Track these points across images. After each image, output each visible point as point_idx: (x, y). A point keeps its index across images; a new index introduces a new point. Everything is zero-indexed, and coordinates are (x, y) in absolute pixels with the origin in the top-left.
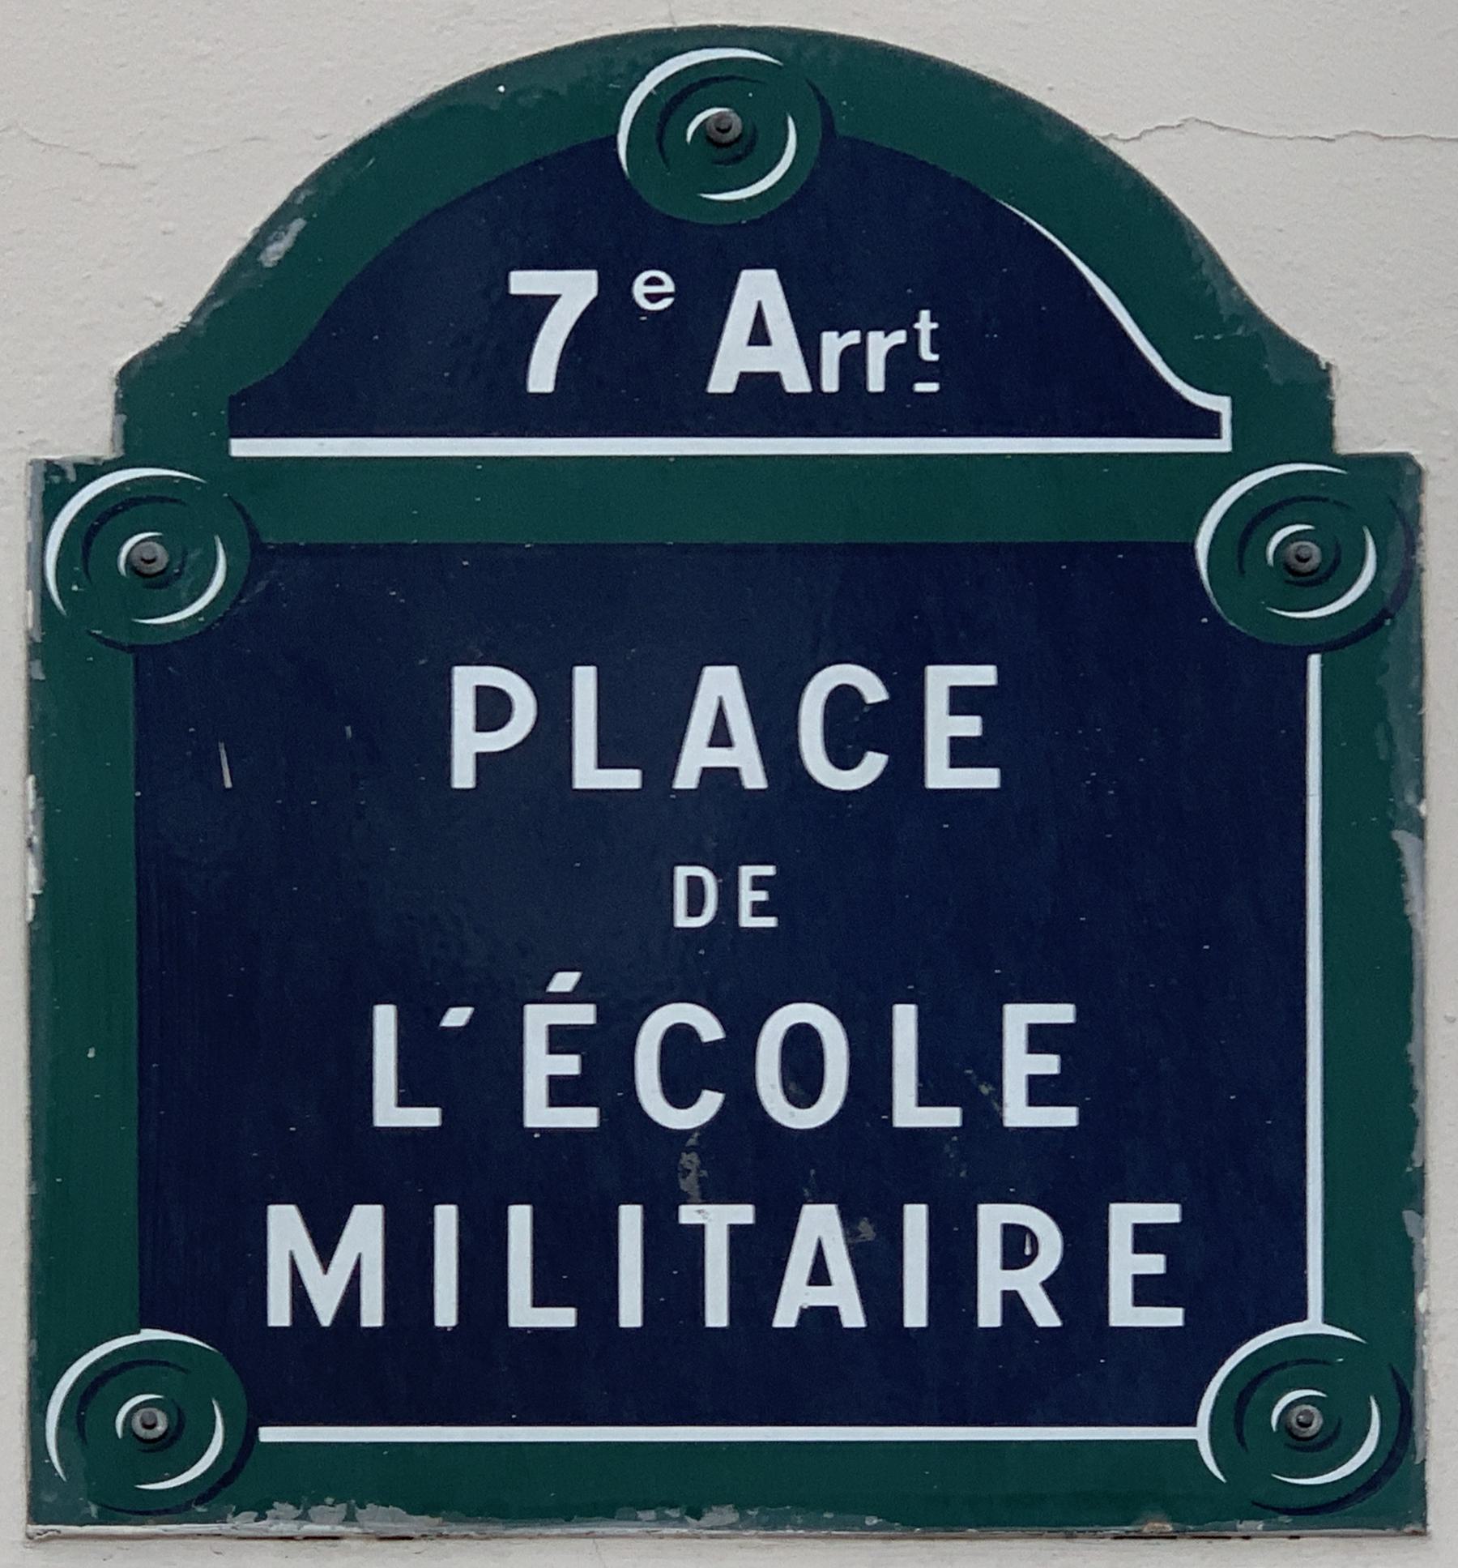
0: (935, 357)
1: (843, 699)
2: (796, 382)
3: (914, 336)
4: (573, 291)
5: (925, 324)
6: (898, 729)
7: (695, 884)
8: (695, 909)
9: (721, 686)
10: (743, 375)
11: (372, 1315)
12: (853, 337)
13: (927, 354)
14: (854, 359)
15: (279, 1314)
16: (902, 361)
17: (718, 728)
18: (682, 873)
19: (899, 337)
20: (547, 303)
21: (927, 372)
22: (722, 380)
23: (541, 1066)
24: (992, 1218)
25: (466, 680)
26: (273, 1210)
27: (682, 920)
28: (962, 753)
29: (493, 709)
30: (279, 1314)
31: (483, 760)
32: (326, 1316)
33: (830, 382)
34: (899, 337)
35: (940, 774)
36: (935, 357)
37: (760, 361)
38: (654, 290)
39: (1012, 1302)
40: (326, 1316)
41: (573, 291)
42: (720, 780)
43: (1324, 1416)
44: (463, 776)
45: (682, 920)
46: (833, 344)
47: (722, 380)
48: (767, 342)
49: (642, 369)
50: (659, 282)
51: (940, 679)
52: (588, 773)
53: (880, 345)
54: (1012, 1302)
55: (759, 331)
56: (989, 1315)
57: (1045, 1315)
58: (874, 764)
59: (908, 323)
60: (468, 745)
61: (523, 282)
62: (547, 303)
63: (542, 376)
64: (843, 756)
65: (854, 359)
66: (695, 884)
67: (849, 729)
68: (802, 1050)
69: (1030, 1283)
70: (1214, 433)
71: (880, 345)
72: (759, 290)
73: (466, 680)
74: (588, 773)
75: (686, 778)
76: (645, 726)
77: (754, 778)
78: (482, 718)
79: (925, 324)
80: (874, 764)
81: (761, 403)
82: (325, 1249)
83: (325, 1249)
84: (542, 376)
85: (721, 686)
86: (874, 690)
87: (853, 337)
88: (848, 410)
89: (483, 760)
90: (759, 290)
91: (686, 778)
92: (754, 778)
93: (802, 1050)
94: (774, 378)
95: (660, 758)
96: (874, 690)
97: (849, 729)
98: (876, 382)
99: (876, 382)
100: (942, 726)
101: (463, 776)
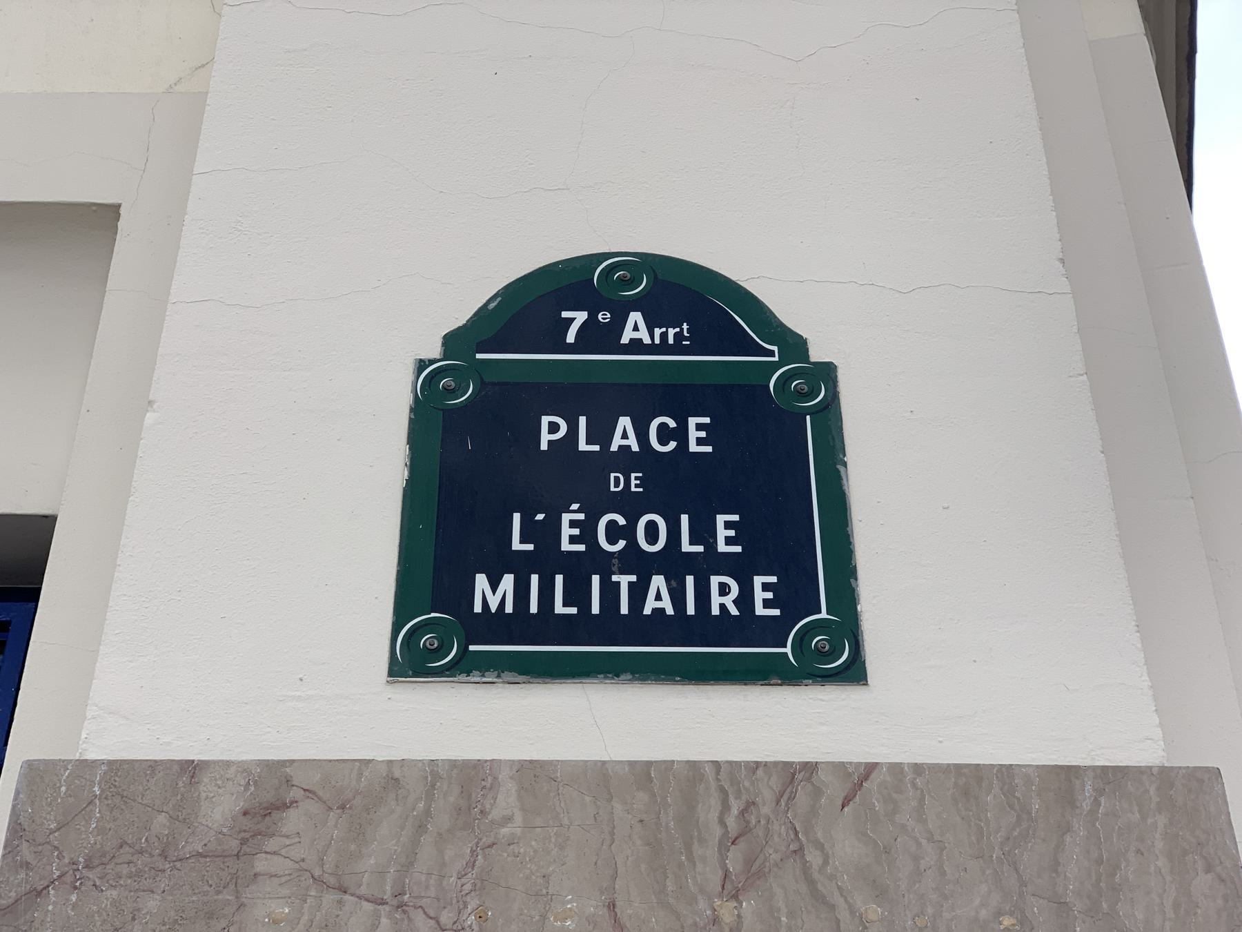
2: (647, 340)
3: (682, 330)
4: (581, 317)
6: (681, 434)
9: (625, 422)
13: (686, 334)
14: (664, 336)
15: (478, 608)
17: (624, 433)
21: (686, 339)
22: (625, 340)
24: (715, 580)
25: (545, 420)
29: (554, 428)
30: (478, 608)
33: (657, 341)
35: (693, 447)
38: (603, 317)
39: (722, 606)
41: (581, 317)
44: (544, 446)
46: (658, 332)
47: (625, 340)
49: (600, 337)
51: (692, 422)
52: (583, 446)
53: (671, 332)
54: (722, 606)
55: (635, 327)
59: (680, 326)
60: (545, 438)
63: (571, 338)
65: (664, 336)
69: (728, 601)
71: (671, 332)
72: (635, 317)
73: (545, 420)
75: (614, 448)
76: (600, 433)
79: (685, 326)
84: (571, 338)
85: (625, 422)
90: (635, 317)
95: (606, 441)
98: (671, 341)
99: (671, 341)
100: (693, 434)
101: (544, 446)
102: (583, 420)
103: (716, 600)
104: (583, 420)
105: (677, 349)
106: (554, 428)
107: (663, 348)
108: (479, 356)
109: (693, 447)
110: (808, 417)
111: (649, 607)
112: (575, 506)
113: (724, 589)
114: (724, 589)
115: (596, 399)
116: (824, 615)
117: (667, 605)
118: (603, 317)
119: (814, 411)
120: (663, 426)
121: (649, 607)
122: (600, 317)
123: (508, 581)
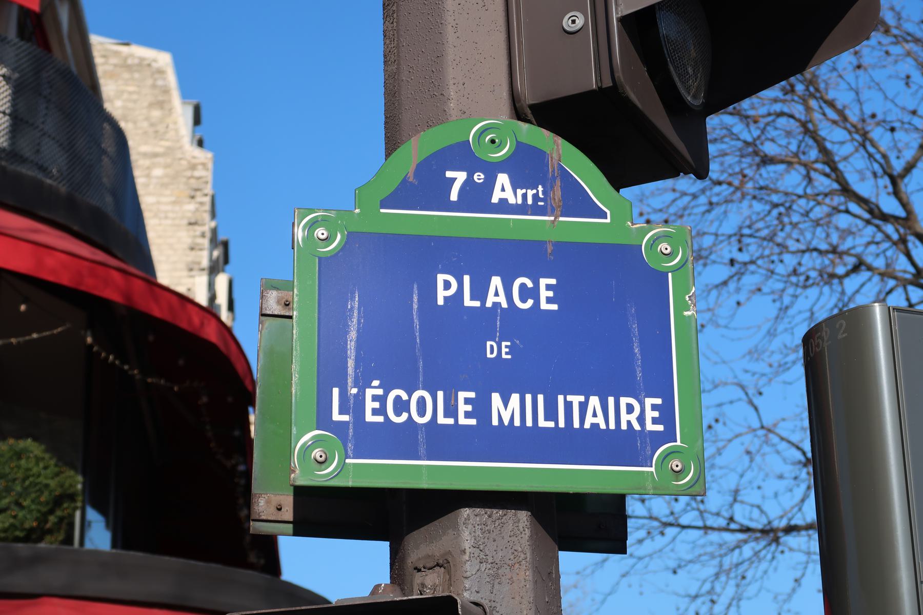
1: (523, 286)
2: (512, 201)
4: (460, 177)
11: (517, 423)
12: (524, 191)
13: (541, 195)
14: (525, 196)
15: (495, 422)
16: (535, 197)
19: (535, 191)
20: (454, 179)
21: (541, 200)
22: (495, 200)
23: (370, 405)
24: (624, 401)
25: (441, 278)
26: (493, 394)
29: (447, 285)
30: (495, 422)
31: (446, 298)
32: (506, 423)
33: (520, 201)
34: (535, 191)
35: (544, 306)
37: (503, 195)
38: (479, 177)
39: (629, 423)
40: (506, 423)
41: (460, 177)
42: (496, 305)
44: (440, 302)
46: (520, 192)
47: (495, 200)
49: (476, 197)
51: (543, 282)
52: (468, 302)
53: (530, 193)
54: (629, 423)
55: (503, 188)
56: (624, 426)
57: (637, 427)
58: (530, 302)
59: (536, 188)
61: (449, 174)
62: (454, 179)
63: (454, 197)
65: (525, 196)
67: (525, 293)
68: (421, 402)
69: (633, 418)
71: (530, 193)
72: (503, 179)
73: (441, 278)
74: (468, 302)
75: (489, 304)
76: (479, 292)
77: (505, 305)
78: (445, 286)
79: (540, 188)
80: (530, 302)
81: (503, 207)
82: (506, 406)
83: (506, 406)
84: (454, 197)
86: (530, 284)
87: (524, 191)
88: (536, 210)
89: (446, 298)
90: (503, 179)
91: (489, 304)
92: (505, 305)
93: (421, 402)
94: (506, 200)
95: (483, 298)
96: (530, 284)
97: (525, 293)
98: (530, 201)
99: (530, 201)
100: (544, 294)
101: (440, 302)
102: (467, 279)
104: (467, 279)
106: (447, 285)
108: (382, 211)
109: (544, 306)
110: (670, 275)
113: (630, 408)
114: (630, 408)
116: (678, 443)
117: (600, 420)
118: (479, 177)
119: (675, 270)
120: (523, 286)
122: (482, 176)
123: (515, 398)
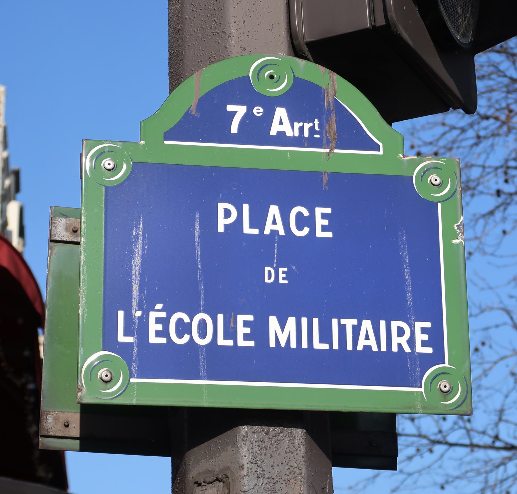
0: (319, 130)
1: (299, 215)
2: (289, 133)
3: (314, 124)
4: (241, 110)
5: (316, 122)
6: (310, 221)
7: (270, 272)
8: (270, 278)
9: (274, 210)
10: (278, 131)
13: (317, 128)
14: (301, 129)
15: (272, 344)
16: (312, 130)
17: (274, 221)
18: (267, 269)
19: (311, 125)
20: (235, 113)
22: (273, 132)
24: (395, 324)
25: (222, 206)
27: (267, 281)
28: (324, 228)
29: (227, 214)
31: (226, 226)
33: (297, 134)
34: (311, 125)
36: (319, 130)
37: (281, 128)
38: (258, 111)
39: (400, 345)
41: (241, 110)
42: (274, 232)
43: (440, 178)
44: (221, 229)
45: (267, 281)
46: (297, 125)
47: (273, 132)
48: (276, 224)
49: (256, 130)
50: (259, 109)
52: (247, 230)
53: (307, 126)
54: (400, 345)
55: (281, 122)
59: (313, 121)
60: (222, 222)
61: (230, 108)
62: (235, 113)
63: (234, 129)
64: (300, 228)
65: (301, 129)
66: (270, 272)
69: (404, 340)
70: (379, 150)
71: (307, 126)
72: (281, 113)
73: (222, 206)
75: (267, 232)
76: (258, 220)
77: (282, 233)
79: (316, 122)
81: (281, 139)
84: (234, 129)
85: (274, 210)
90: (281, 113)
91: (267, 232)
92: (282, 233)
95: (262, 229)
96: (306, 213)
97: (301, 221)
98: (306, 134)
99: (306, 134)
100: (320, 222)
101: (221, 229)
102: (246, 207)
103: (395, 340)
104: (246, 207)
105: (312, 142)
106: (227, 214)
107: (299, 141)
111: (362, 343)
112: (159, 306)
113: (401, 332)
115: (262, 188)
116: (447, 365)
117: (372, 343)
121: (362, 343)
